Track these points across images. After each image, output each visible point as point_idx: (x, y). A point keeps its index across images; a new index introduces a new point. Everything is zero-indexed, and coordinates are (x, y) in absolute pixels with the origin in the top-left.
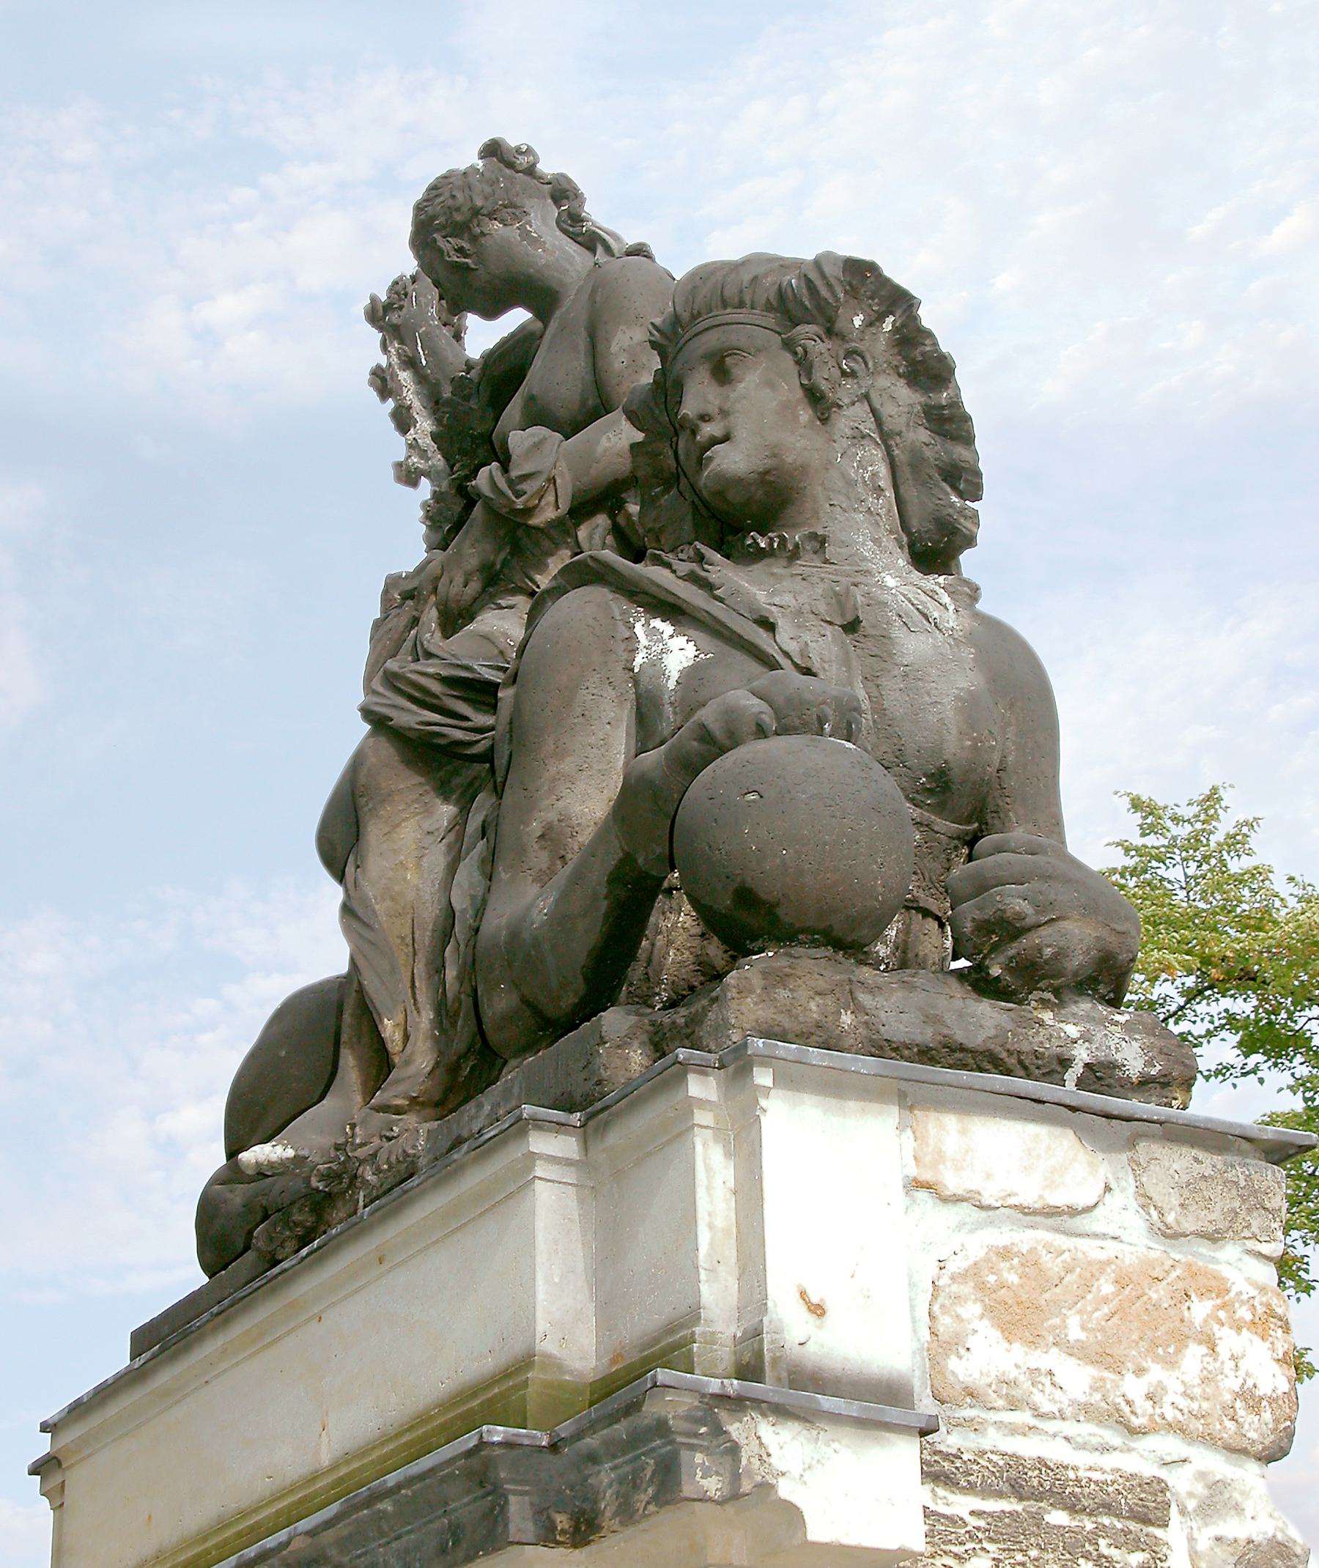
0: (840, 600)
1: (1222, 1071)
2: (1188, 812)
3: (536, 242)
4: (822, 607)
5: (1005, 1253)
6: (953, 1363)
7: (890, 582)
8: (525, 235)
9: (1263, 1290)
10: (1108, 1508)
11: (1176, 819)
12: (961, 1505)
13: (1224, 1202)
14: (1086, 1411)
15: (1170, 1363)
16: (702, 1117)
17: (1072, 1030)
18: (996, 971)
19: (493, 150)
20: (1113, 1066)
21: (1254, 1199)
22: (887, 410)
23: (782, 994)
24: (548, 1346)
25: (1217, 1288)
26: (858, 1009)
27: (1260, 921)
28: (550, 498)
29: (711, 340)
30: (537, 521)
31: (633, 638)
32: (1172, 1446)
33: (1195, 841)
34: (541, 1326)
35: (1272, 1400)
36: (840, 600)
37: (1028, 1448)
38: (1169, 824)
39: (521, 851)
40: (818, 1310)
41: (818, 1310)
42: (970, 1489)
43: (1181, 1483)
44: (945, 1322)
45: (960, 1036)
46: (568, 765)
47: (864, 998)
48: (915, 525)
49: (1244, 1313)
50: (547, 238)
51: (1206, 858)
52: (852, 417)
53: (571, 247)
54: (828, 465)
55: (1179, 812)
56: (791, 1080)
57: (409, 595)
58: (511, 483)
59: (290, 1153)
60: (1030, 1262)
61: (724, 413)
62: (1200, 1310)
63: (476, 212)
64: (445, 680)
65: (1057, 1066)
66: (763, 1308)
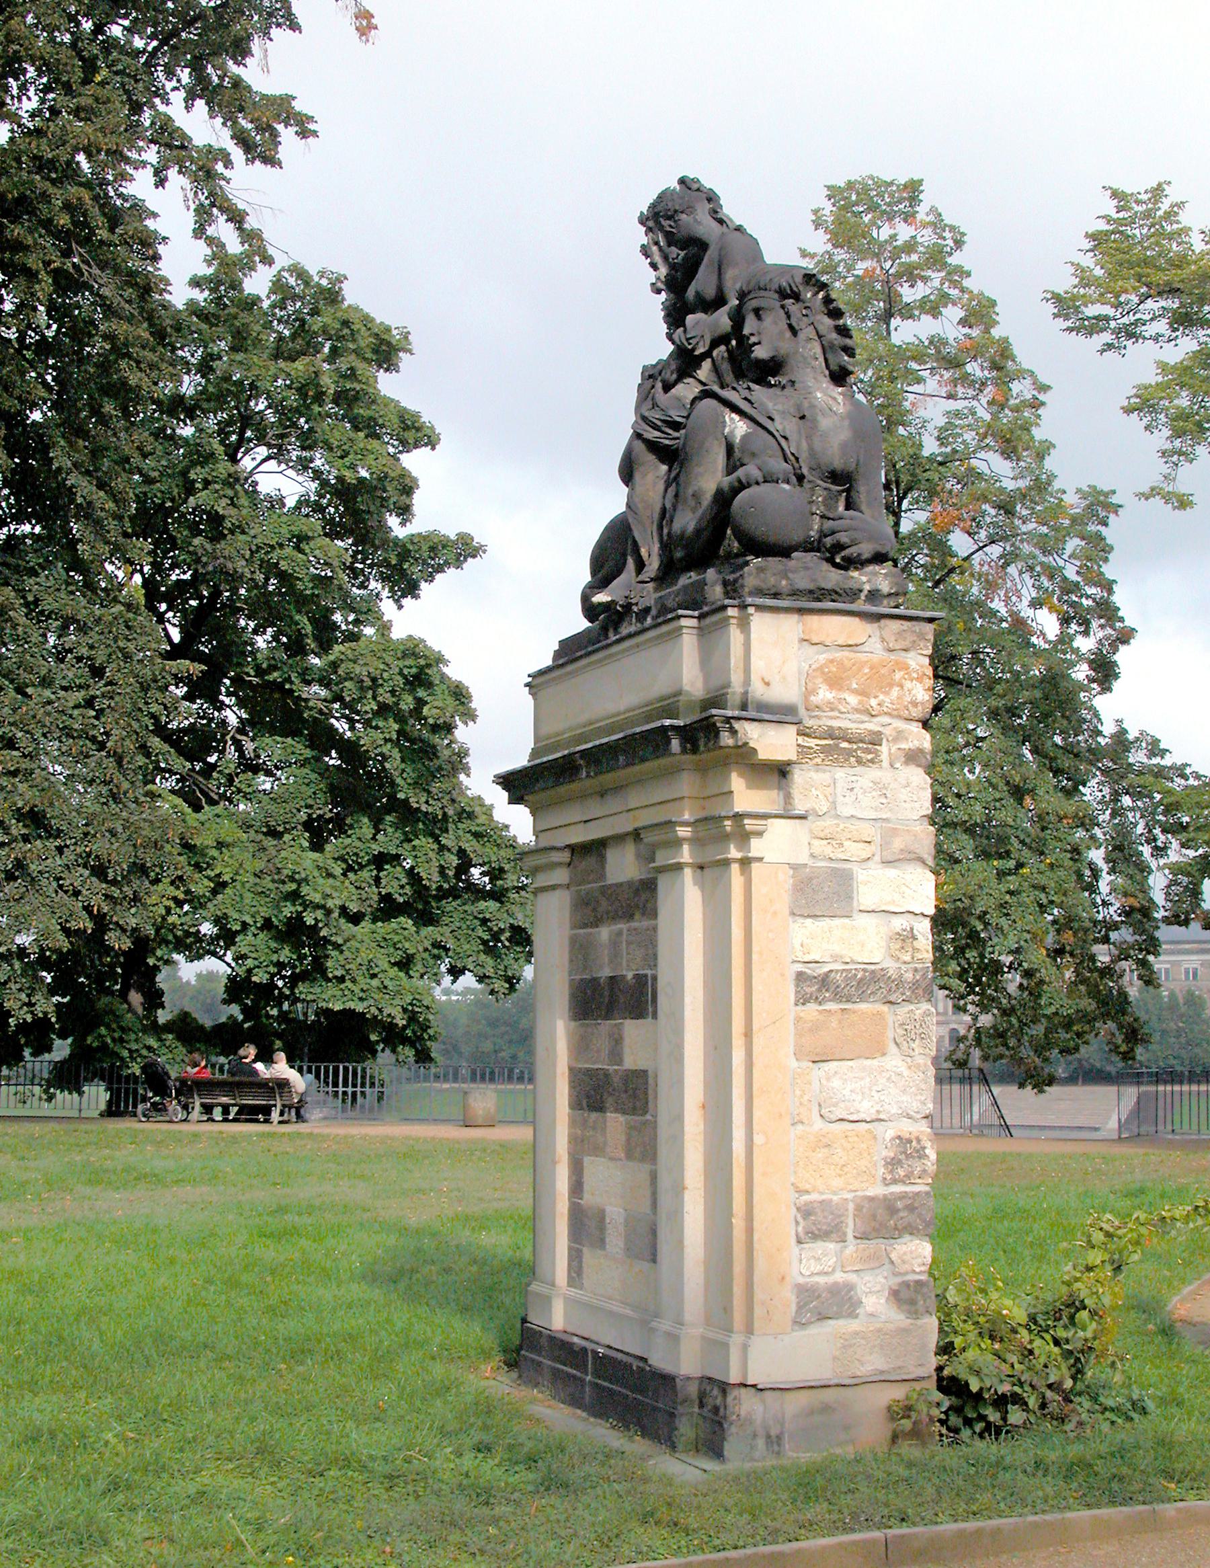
0: (799, 407)
1: (1156, 338)
2: (1144, 197)
3: (699, 223)
4: (792, 410)
5: (832, 661)
6: (812, 698)
7: (819, 395)
8: (696, 220)
9: (922, 666)
10: (862, 741)
11: (1138, 202)
12: (812, 742)
13: (910, 638)
14: (857, 711)
15: (887, 693)
16: (733, 621)
17: (864, 579)
18: (838, 560)
19: (682, 181)
20: (878, 590)
21: (922, 636)
22: (820, 328)
23: (762, 575)
24: (686, 687)
25: (905, 667)
26: (788, 578)
27: (1180, 262)
28: (701, 343)
29: (754, 304)
30: (697, 353)
31: (725, 422)
32: (886, 720)
33: (1147, 215)
34: (685, 681)
35: (922, 704)
36: (799, 407)
37: (835, 724)
38: (1134, 205)
39: (685, 501)
40: (768, 684)
41: (768, 684)
42: (816, 738)
43: (887, 731)
44: (810, 685)
45: (823, 585)
46: (701, 469)
47: (790, 575)
48: (831, 367)
49: (915, 675)
50: (704, 222)
51: (1153, 225)
52: (807, 332)
53: (714, 224)
54: (797, 352)
55: (1140, 197)
56: (760, 608)
57: (651, 376)
58: (688, 339)
59: (609, 599)
60: (840, 664)
61: (759, 333)
62: (898, 675)
63: (676, 211)
64: (663, 421)
65: (854, 594)
66: (749, 685)
